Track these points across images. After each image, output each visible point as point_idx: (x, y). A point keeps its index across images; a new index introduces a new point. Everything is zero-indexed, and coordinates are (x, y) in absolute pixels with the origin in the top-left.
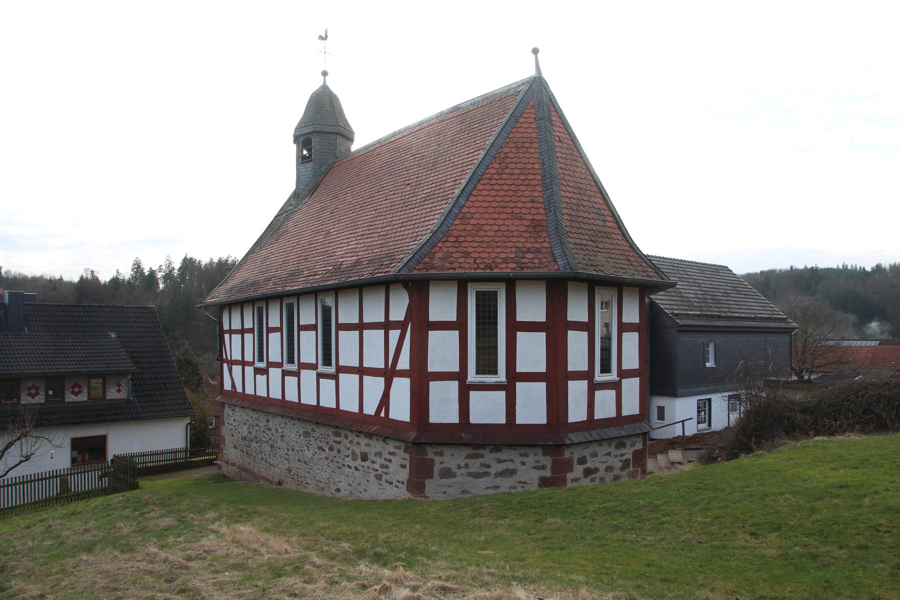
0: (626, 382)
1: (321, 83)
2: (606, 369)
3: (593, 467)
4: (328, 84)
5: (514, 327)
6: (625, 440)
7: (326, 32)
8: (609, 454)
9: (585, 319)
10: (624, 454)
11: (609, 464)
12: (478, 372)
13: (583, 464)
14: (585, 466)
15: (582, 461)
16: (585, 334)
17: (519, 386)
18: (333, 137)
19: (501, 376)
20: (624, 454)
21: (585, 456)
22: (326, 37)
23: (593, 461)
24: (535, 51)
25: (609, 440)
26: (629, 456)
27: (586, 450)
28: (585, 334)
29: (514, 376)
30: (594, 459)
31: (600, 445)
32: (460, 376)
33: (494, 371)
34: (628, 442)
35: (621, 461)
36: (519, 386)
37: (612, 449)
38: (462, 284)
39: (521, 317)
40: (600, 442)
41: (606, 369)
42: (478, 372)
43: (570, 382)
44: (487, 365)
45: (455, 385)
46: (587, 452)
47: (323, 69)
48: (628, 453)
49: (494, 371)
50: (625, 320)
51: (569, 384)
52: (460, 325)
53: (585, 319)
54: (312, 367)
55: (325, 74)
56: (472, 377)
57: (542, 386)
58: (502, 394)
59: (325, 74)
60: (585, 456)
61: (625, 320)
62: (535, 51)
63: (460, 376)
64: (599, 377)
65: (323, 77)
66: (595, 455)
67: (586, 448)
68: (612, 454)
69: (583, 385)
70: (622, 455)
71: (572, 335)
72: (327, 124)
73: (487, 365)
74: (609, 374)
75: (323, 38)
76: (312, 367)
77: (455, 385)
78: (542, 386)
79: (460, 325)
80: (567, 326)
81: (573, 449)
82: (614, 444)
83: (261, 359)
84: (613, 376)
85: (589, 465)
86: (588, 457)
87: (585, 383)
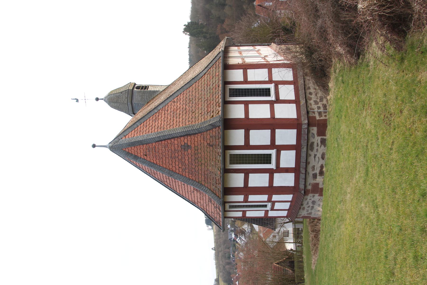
0: (276, 78)
1: (103, 101)
2: (267, 92)
3: (320, 169)
4: (103, 97)
5: (246, 82)
6: (309, 144)
7: (73, 99)
8: (315, 156)
9: (242, 176)
10: (318, 144)
11: (320, 156)
12: (270, 163)
13: (317, 176)
14: (318, 174)
15: (315, 176)
16: (251, 175)
17: (277, 143)
18: (134, 105)
19: (273, 152)
20: (318, 144)
21: (313, 174)
22: (76, 99)
23: (316, 169)
24: (94, 146)
25: (308, 155)
26: (319, 138)
27: (309, 175)
28: (251, 175)
29: (273, 145)
30: (315, 168)
31: (309, 163)
32: (271, 172)
33: (269, 90)
34: (312, 140)
35: (321, 146)
36: (277, 143)
37: (312, 154)
38: (226, 171)
39: (242, 79)
40: (307, 163)
41: (267, 92)
42: (270, 163)
43: (274, 185)
44: (267, 159)
45: (276, 175)
46: (311, 173)
47: (95, 100)
48: (317, 139)
49: (269, 90)
50: (242, 143)
51: (277, 118)
52: (246, 104)
53: (242, 176)
54: (267, 212)
55: (97, 99)
56: (272, 166)
57: (277, 131)
58: (283, 152)
59: (97, 99)
60: (313, 174)
61: (242, 143)
62: (94, 146)
63: (272, 103)
64: (272, 98)
65: (99, 100)
66: (313, 167)
67: (309, 174)
68: (316, 153)
69: (276, 176)
70: (318, 146)
71: (252, 116)
72: (127, 108)
73: (267, 159)
74: (272, 155)
75: (77, 101)
76: (267, 212)
77: (276, 175)
78: (277, 131)
79: (247, 172)
80: (246, 187)
81: (308, 184)
82: (310, 152)
83: (266, 206)
84: (272, 87)
85: (317, 171)
86: (314, 172)
87: (275, 105)
